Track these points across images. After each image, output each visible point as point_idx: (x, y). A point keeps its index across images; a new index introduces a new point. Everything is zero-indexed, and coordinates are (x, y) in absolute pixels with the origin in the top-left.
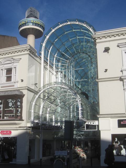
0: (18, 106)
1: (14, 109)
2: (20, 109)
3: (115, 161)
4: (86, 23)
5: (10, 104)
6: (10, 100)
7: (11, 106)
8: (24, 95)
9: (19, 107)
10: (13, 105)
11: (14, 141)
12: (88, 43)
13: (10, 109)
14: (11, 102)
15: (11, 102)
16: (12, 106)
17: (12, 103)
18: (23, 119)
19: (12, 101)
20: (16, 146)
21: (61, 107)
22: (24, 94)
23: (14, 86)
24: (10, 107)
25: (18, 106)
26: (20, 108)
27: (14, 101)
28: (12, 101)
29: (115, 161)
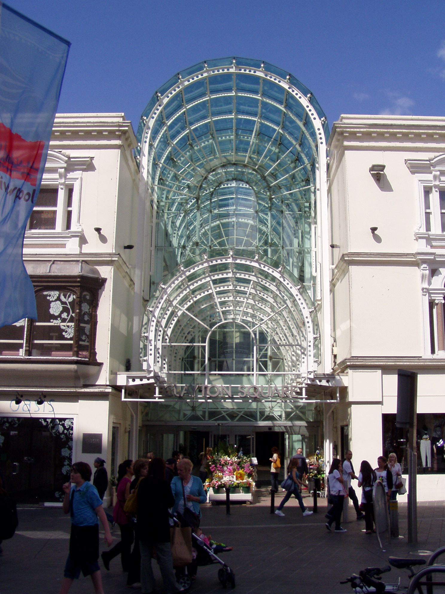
0: (85, 314)
1: (70, 324)
2: (88, 327)
3: (88, 318)
4: (310, 98)
5: (55, 308)
6: (52, 293)
7: (57, 314)
8: (104, 281)
9: (86, 318)
10: (65, 310)
11: (61, 431)
12: (191, 145)
13: (54, 323)
14: (58, 299)
15: (56, 300)
16: (62, 312)
17: (63, 303)
18: (99, 359)
19: (62, 298)
20: (70, 448)
21: (439, 426)
22: (346, 385)
23: (63, 246)
24: (55, 318)
25: (85, 314)
26: (87, 322)
27: (71, 299)
28: (62, 298)
29: (88, 318)
